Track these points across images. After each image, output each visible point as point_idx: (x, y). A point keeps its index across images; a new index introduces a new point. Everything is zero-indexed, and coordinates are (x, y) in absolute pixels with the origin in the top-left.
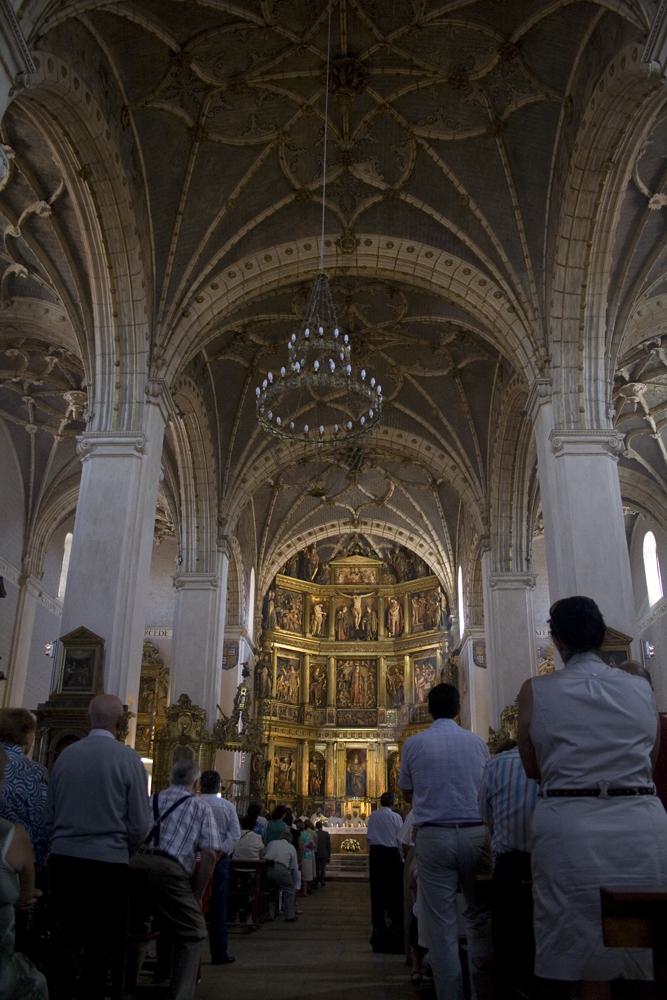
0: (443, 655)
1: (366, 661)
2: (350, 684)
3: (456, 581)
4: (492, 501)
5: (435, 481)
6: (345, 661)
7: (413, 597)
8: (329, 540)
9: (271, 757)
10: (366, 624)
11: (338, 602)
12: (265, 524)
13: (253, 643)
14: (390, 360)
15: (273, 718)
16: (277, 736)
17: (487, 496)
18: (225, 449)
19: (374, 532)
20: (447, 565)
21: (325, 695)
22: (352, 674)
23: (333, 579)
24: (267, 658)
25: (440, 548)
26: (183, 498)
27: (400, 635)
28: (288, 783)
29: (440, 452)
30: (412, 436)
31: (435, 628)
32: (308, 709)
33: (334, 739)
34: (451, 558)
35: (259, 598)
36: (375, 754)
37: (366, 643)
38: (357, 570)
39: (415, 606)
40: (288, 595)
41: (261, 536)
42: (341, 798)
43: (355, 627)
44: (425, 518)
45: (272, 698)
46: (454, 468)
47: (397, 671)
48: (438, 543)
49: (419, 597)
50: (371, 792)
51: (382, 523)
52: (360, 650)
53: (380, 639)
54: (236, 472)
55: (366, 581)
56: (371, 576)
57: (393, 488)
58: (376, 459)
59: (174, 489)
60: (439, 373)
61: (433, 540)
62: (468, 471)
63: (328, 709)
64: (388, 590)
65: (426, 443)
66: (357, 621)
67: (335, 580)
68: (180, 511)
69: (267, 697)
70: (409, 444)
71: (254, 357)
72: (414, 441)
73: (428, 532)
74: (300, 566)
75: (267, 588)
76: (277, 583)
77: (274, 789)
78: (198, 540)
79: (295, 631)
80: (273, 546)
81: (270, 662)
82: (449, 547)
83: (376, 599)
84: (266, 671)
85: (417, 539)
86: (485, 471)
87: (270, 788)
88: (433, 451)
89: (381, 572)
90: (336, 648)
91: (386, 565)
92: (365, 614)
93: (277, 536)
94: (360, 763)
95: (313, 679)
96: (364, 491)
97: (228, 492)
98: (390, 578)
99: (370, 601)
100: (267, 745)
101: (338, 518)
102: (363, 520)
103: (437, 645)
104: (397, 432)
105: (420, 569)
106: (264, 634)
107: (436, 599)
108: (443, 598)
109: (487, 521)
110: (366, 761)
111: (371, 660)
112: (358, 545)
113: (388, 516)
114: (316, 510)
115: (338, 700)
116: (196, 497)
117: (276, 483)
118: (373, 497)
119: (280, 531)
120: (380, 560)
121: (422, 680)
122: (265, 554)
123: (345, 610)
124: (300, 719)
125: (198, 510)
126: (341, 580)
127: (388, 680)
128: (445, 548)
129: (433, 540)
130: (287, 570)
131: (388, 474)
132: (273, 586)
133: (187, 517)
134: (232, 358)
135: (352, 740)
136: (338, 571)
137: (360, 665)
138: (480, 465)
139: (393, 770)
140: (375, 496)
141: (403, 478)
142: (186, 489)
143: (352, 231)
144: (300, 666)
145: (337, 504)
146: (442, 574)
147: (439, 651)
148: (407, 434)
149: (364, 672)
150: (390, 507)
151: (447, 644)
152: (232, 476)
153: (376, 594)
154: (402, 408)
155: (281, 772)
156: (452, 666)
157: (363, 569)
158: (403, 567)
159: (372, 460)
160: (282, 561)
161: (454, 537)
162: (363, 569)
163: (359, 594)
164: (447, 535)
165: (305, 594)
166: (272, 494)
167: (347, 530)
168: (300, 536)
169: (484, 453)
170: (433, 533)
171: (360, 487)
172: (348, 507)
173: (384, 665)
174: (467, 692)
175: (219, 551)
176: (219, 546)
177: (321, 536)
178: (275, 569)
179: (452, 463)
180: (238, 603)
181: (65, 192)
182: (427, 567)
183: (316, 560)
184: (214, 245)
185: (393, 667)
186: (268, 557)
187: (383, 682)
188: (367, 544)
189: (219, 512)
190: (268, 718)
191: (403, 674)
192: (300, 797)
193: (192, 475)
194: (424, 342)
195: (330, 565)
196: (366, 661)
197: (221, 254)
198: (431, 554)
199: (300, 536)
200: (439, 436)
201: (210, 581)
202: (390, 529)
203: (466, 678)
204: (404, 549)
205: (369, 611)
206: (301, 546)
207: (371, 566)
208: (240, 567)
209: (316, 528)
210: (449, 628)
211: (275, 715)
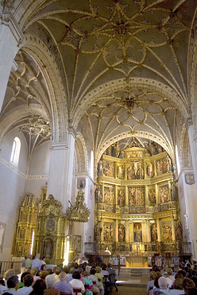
0: (171, 184)
1: (140, 187)
2: (134, 197)
3: (175, 152)
4: (191, 101)
5: (163, 111)
6: (131, 188)
7: (157, 161)
8: (123, 140)
9: (102, 226)
10: (139, 173)
11: (128, 165)
12: (96, 134)
13: (94, 181)
14: (139, 40)
15: (103, 211)
16: (106, 218)
17: (189, 100)
18: (71, 90)
19: (140, 136)
20: (171, 146)
21: (124, 202)
22: (134, 193)
23: (125, 156)
24: (100, 187)
25: (167, 139)
26: (52, 111)
27: (153, 177)
28: (110, 237)
29: (165, 85)
30: (152, 80)
31: (167, 172)
32: (117, 207)
33: (128, 219)
34: (172, 143)
35: (96, 163)
36: (145, 224)
37: (140, 180)
38: (135, 152)
39: (158, 165)
40: (108, 163)
41: (95, 138)
42: (132, 242)
43: (135, 174)
44: (160, 128)
45: (102, 203)
46: (172, 91)
47: (153, 191)
48: (166, 137)
49: (160, 161)
51: (143, 132)
52: (138, 183)
53: (145, 178)
54: (76, 100)
55: (138, 156)
56: (140, 155)
57: (146, 116)
58: (139, 103)
59: (49, 107)
60: (163, 44)
61: (164, 137)
62: (179, 91)
63: (125, 207)
64: (147, 159)
65: (159, 82)
66: (136, 172)
67: (126, 157)
68: (52, 117)
69: (100, 202)
70: (152, 84)
71: (100, 113)
72: (153, 82)
73: (162, 133)
74: (112, 151)
75: (99, 160)
76: (103, 158)
77: (104, 239)
78: (59, 129)
79: (111, 176)
80: (100, 143)
81: (101, 188)
82: (171, 138)
83: (143, 163)
84: (99, 192)
85: (158, 137)
86: (187, 89)
87: (102, 239)
88: (162, 85)
89: (144, 153)
90: (128, 182)
91: (146, 150)
92: (139, 169)
93: (102, 139)
94: (139, 228)
95: (119, 195)
96: (135, 119)
97: (73, 109)
98: (148, 154)
99: (140, 164)
100: (101, 221)
101: (126, 131)
102: (136, 131)
103: (168, 179)
104: (146, 79)
105: (160, 150)
106: (98, 178)
107: (167, 161)
108: (170, 160)
109: (190, 112)
111: (142, 187)
112: (135, 142)
113: (146, 129)
114: (117, 128)
115: (129, 203)
116: (58, 109)
117: (99, 116)
118: (139, 121)
119: (103, 137)
120: (144, 148)
121: (163, 194)
122: (97, 147)
123: (131, 168)
124: (114, 211)
125: (59, 115)
126: (129, 157)
127: (149, 195)
128: (170, 141)
129: (164, 137)
130: (107, 153)
131: (144, 110)
132: (102, 159)
133: (55, 119)
134: (68, 44)
135: (136, 219)
136: (127, 153)
137: (138, 189)
138: (185, 87)
139: (153, 231)
140: (140, 121)
141: (150, 111)
142: (53, 106)
143: (128, 77)
144: (114, 190)
145: (125, 125)
146: (169, 150)
147: (169, 182)
148: (150, 79)
149: (139, 192)
150: (146, 124)
151: (172, 178)
152: (74, 101)
153: (143, 161)
154: (147, 67)
155: (107, 232)
156: (175, 187)
157: (137, 152)
158: (153, 150)
159: (137, 104)
160: (105, 149)
161: (173, 134)
162: (137, 152)
163: (136, 162)
164: (170, 134)
165: (115, 162)
166: (98, 121)
167: (129, 136)
168: (111, 139)
169: (186, 82)
170: (164, 133)
171: (133, 117)
172: (129, 126)
173: (147, 189)
174: (183, 196)
175: (69, 133)
176: (69, 131)
177: (120, 139)
178: (102, 152)
179: (171, 89)
180: (85, 163)
181: (40, 73)
182: (162, 148)
183: (118, 149)
184: (87, 84)
185: (151, 189)
186: (99, 147)
187: (147, 196)
188: (138, 142)
189: (69, 117)
190: (101, 210)
191: (155, 192)
192: (115, 242)
193: (55, 99)
194: (154, 26)
195: (124, 151)
196: (140, 187)
197: (88, 87)
198: (164, 143)
199: (111, 139)
200: (164, 78)
201: (65, 146)
202: (147, 134)
203: (182, 190)
204: (153, 143)
205: (140, 168)
206: (112, 143)
207: (140, 151)
208: (86, 152)
209: (117, 136)
210: (173, 172)
211: (103, 209)
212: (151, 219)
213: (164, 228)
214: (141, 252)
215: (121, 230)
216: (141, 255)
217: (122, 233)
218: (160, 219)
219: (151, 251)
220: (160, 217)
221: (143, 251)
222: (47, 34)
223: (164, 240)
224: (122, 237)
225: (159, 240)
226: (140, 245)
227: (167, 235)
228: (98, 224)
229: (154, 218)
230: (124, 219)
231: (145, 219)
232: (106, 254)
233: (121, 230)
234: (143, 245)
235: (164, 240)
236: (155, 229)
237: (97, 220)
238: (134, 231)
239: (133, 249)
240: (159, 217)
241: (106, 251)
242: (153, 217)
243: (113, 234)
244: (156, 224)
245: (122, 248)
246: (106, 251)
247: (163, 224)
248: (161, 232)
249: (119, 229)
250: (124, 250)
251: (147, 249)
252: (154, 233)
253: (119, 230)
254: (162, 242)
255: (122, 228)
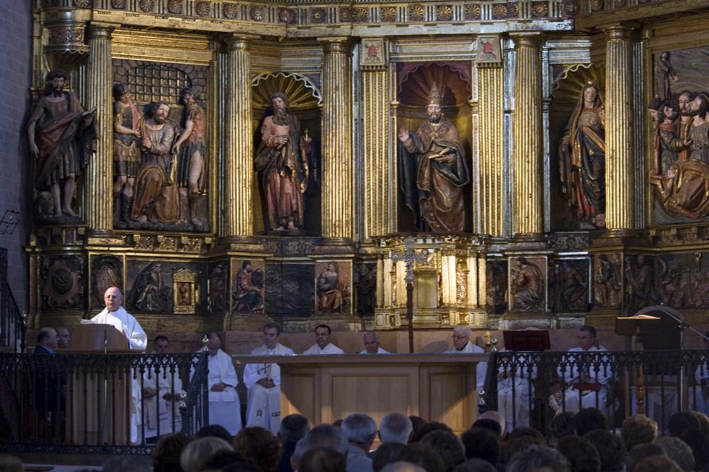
9: (101, 103)
33: (345, 29)
42: (376, 241)
50: (488, 218)
87: (101, 210)
110: (469, 107)
135: (412, 29)
139: (571, 137)
155: (147, 155)
192: (224, 241)
212: (553, 26)
213: (669, 112)
214: (455, 317)
215: (282, 130)
216: (444, 345)
217: (290, 163)
218: (634, 31)
219: (540, 314)
220: (633, 15)
221: (469, 317)
222: (552, 289)
223: (661, 218)
224: (290, 189)
225: (615, 215)
226: (448, 265)
227: (689, 176)
228: (60, 82)
229: (582, 25)
230: (306, 33)
231: (499, 27)
232: (99, 346)
233: (282, 130)
234: (471, 262)
235: (661, 218)
236: (587, 119)
237: (53, 50)
238: (405, 137)
239: (388, 301)
240: (624, 15)
241: (104, 317)
242: (571, 15)
243: (207, 167)
244: (595, 72)
245: (292, 287)
246: (104, 317)
247: (659, 79)
248: (636, 145)
249: (269, 121)
250: (304, 310)
251: (509, 299)
252: (577, 158)
253: (267, 136)
254: (642, 234)
255: (288, 111)
